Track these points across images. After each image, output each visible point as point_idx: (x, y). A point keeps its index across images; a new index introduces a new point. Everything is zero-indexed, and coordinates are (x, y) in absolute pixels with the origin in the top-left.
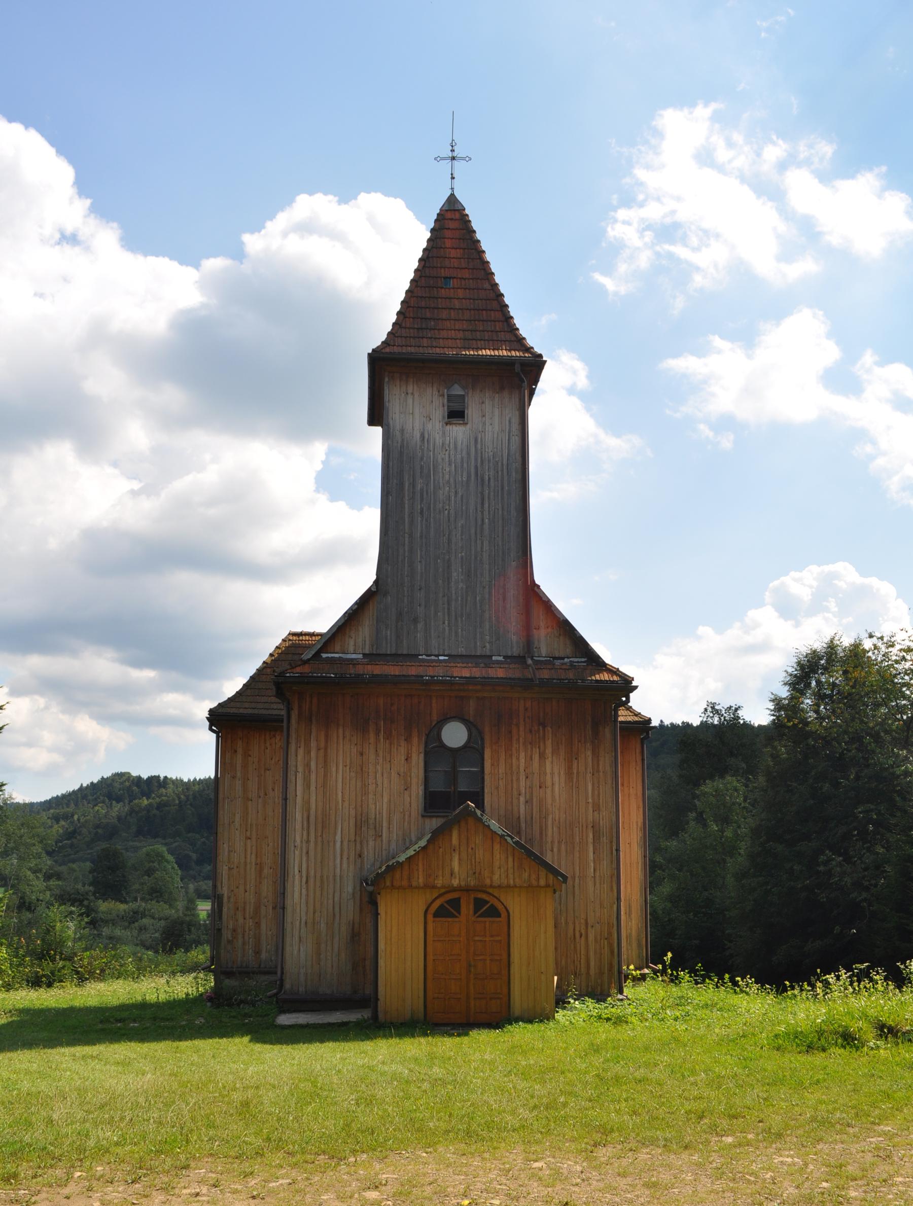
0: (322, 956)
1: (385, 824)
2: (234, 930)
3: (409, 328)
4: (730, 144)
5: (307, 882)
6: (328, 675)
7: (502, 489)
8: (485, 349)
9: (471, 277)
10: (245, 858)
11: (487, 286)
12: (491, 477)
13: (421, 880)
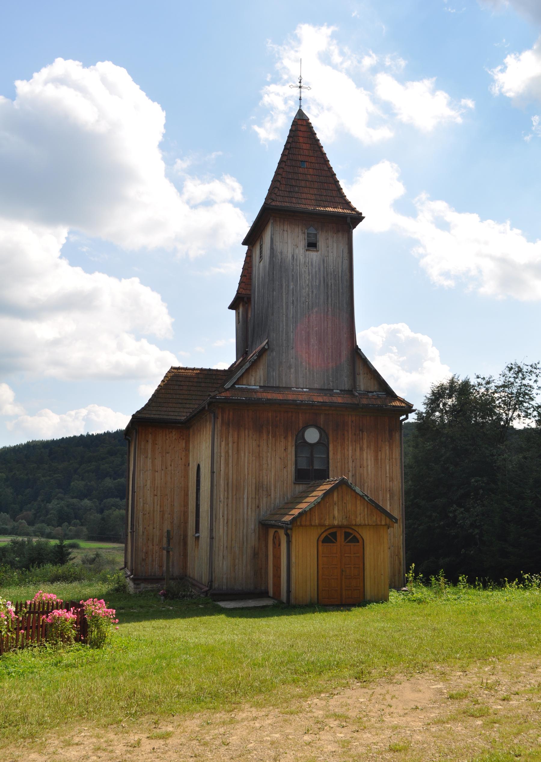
0: (236, 567)
1: (273, 488)
2: (147, 553)
3: (284, 191)
4: (342, 53)
5: (227, 523)
6: (241, 398)
7: (339, 291)
8: (329, 207)
9: (316, 162)
10: (154, 508)
11: (326, 168)
12: (332, 283)
13: (317, 522)
